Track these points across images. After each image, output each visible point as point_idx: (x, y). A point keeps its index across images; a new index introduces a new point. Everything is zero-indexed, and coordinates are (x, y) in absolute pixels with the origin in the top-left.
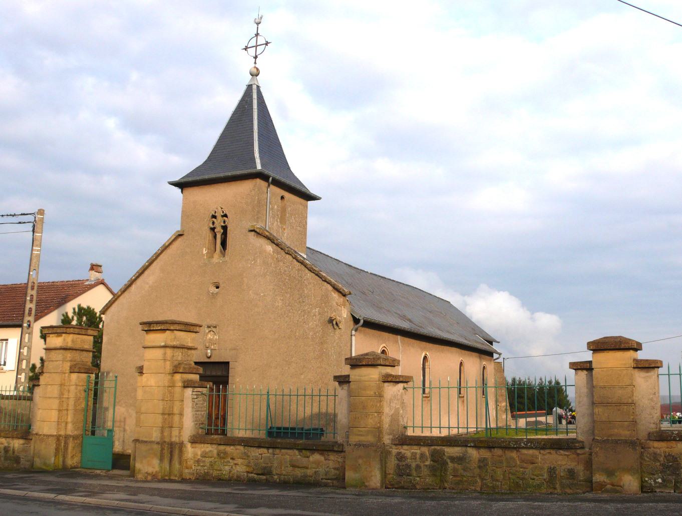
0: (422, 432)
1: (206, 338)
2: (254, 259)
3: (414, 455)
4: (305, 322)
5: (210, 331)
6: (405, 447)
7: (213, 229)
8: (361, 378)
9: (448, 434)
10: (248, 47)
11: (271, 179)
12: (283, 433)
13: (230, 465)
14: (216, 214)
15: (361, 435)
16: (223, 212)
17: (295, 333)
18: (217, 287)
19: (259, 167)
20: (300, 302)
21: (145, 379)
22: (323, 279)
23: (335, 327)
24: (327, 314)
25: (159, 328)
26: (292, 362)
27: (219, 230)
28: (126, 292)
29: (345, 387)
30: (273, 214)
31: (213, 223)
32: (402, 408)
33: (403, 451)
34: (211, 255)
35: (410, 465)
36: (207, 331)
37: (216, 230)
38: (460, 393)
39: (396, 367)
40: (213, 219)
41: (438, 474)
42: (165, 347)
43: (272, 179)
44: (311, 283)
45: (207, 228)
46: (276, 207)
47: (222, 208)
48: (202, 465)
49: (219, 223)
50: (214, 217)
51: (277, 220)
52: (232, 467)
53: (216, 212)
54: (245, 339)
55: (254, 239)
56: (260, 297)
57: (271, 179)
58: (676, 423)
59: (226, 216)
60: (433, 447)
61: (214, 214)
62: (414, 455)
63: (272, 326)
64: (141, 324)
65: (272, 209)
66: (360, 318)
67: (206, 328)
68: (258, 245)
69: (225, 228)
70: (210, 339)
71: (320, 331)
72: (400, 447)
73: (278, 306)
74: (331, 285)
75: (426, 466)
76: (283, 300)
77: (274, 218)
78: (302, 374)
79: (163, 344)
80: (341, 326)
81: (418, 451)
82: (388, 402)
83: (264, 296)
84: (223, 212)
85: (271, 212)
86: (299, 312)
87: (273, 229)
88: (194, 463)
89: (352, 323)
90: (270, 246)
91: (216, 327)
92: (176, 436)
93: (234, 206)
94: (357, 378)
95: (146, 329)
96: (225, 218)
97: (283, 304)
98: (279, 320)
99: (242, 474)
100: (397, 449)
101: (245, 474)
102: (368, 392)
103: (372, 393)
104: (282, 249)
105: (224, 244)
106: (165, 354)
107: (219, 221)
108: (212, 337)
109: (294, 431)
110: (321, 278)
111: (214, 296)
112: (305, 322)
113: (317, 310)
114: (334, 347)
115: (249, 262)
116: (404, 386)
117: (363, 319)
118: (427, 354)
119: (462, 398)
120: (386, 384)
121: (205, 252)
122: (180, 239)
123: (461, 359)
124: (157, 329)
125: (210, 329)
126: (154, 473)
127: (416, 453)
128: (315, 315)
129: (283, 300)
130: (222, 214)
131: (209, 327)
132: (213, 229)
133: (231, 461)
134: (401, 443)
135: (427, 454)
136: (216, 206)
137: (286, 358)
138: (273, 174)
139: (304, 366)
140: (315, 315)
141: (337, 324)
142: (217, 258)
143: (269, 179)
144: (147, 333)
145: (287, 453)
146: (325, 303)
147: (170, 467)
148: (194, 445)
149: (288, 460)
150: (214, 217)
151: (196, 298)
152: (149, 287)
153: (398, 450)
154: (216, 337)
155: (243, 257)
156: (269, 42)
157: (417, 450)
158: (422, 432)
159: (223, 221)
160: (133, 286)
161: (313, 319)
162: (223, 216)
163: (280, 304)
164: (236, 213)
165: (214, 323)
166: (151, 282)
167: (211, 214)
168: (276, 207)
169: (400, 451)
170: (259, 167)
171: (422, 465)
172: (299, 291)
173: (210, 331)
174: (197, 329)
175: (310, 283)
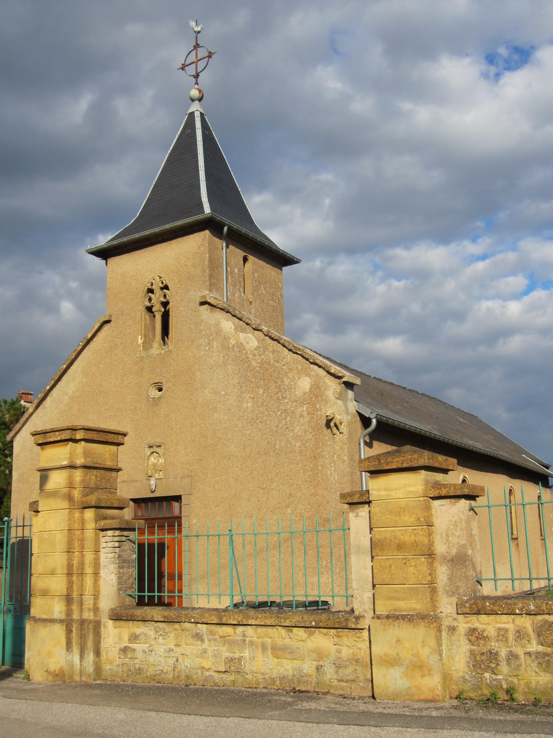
0: (209, 603)
1: (148, 463)
2: (209, 344)
3: (502, 634)
4: (287, 428)
5: (153, 452)
6: (483, 618)
7: (149, 309)
8: (391, 493)
9: (529, 589)
10: (187, 63)
11: (226, 229)
12: (168, 596)
13: (173, 657)
14: (154, 287)
15: (398, 599)
16: (162, 283)
17: (275, 445)
18: (160, 390)
19: (207, 210)
20: (278, 399)
21: (42, 520)
22: (311, 361)
23: (334, 429)
24: (320, 413)
25: (59, 438)
26: (272, 489)
27: (158, 308)
28: (39, 409)
29: (363, 511)
30: (232, 281)
31: (150, 300)
32: (471, 544)
33: (477, 625)
34: (147, 345)
35: (496, 654)
36: (149, 453)
37: (154, 309)
38: (512, 534)
39: (450, 473)
40: (150, 294)
41: (475, 643)
42: (72, 467)
43: (228, 229)
44: (293, 370)
45: (141, 307)
46: (236, 271)
47: (160, 278)
48: (130, 656)
49: (157, 298)
50: (151, 291)
51: (239, 289)
52: (177, 660)
53: (152, 284)
54: (201, 460)
55: (207, 315)
56: (221, 397)
57: (226, 229)
58: (72, 610)
59: (166, 287)
60: (540, 618)
61: (150, 287)
62: (502, 634)
63: (240, 437)
64: (33, 435)
65: (232, 272)
66: (371, 417)
67: (146, 449)
68: (214, 322)
69: (165, 304)
70: (154, 465)
71: (311, 439)
72: (474, 618)
73: (247, 408)
74: (324, 369)
75: (529, 654)
76: (253, 398)
77: (234, 286)
78: (288, 507)
79: (65, 463)
80: (342, 428)
81: (511, 626)
82: (444, 535)
83: (226, 394)
84: (162, 283)
85: (229, 277)
86: (279, 413)
87: (234, 302)
88: (119, 654)
89: (359, 424)
90: (230, 322)
91: (160, 446)
92: (89, 610)
93: (176, 273)
94: (383, 493)
95: (41, 442)
96: (165, 290)
97: (254, 403)
98: (250, 427)
99: (195, 671)
100: (467, 623)
101: (199, 671)
102: (406, 518)
103: (412, 519)
104: (248, 324)
105: (165, 331)
106: (70, 478)
107: (158, 296)
108: (155, 462)
109: (173, 594)
110: (307, 360)
111: (156, 402)
112: (287, 428)
113: (305, 409)
114: (334, 462)
115: (202, 348)
116: (470, 504)
117: (376, 417)
118: (467, 476)
119: (516, 540)
120: (437, 503)
121: (140, 341)
122: (106, 327)
123: (510, 485)
124: (55, 439)
125: (152, 450)
126: (57, 673)
127: (507, 630)
128: (302, 416)
129: (253, 398)
130: (162, 286)
131: (150, 447)
132: (149, 309)
133: (175, 649)
134: (475, 612)
135: (530, 630)
136: (152, 276)
137: (263, 484)
138: (229, 222)
139: (290, 494)
140: (302, 416)
141: (336, 426)
142: (156, 348)
143: (223, 229)
144: (42, 449)
145: (266, 635)
146: (317, 396)
147: (81, 661)
148: (118, 623)
149: (269, 643)
150: (151, 291)
151: (132, 407)
152: (70, 398)
153: (469, 625)
154: (162, 461)
155: (193, 341)
156: (212, 52)
157: (506, 622)
158: (209, 603)
159: (163, 295)
160: (48, 399)
161: (299, 422)
162: (162, 289)
163: (250, 405)
164: (179, 282)
165: (158, 441)
166: (70, 392)
167: (146, 288)
168: (236, 271)
169: (473, 627)
170: (207, 210)
171: (520, 651)
172: (276, 383)
173: (153, 452)
174: (120, 439)
175: (291, 370)
